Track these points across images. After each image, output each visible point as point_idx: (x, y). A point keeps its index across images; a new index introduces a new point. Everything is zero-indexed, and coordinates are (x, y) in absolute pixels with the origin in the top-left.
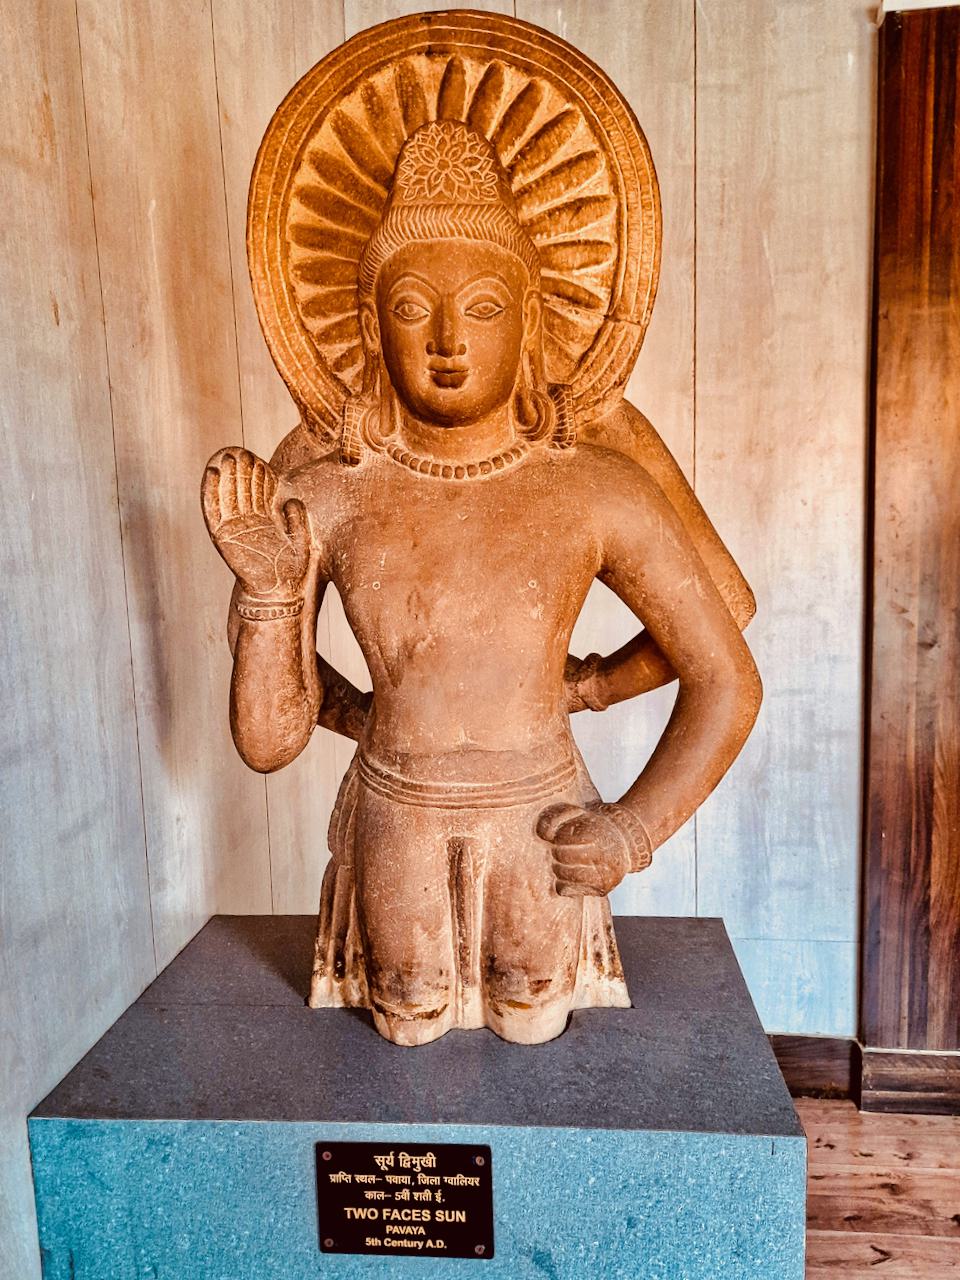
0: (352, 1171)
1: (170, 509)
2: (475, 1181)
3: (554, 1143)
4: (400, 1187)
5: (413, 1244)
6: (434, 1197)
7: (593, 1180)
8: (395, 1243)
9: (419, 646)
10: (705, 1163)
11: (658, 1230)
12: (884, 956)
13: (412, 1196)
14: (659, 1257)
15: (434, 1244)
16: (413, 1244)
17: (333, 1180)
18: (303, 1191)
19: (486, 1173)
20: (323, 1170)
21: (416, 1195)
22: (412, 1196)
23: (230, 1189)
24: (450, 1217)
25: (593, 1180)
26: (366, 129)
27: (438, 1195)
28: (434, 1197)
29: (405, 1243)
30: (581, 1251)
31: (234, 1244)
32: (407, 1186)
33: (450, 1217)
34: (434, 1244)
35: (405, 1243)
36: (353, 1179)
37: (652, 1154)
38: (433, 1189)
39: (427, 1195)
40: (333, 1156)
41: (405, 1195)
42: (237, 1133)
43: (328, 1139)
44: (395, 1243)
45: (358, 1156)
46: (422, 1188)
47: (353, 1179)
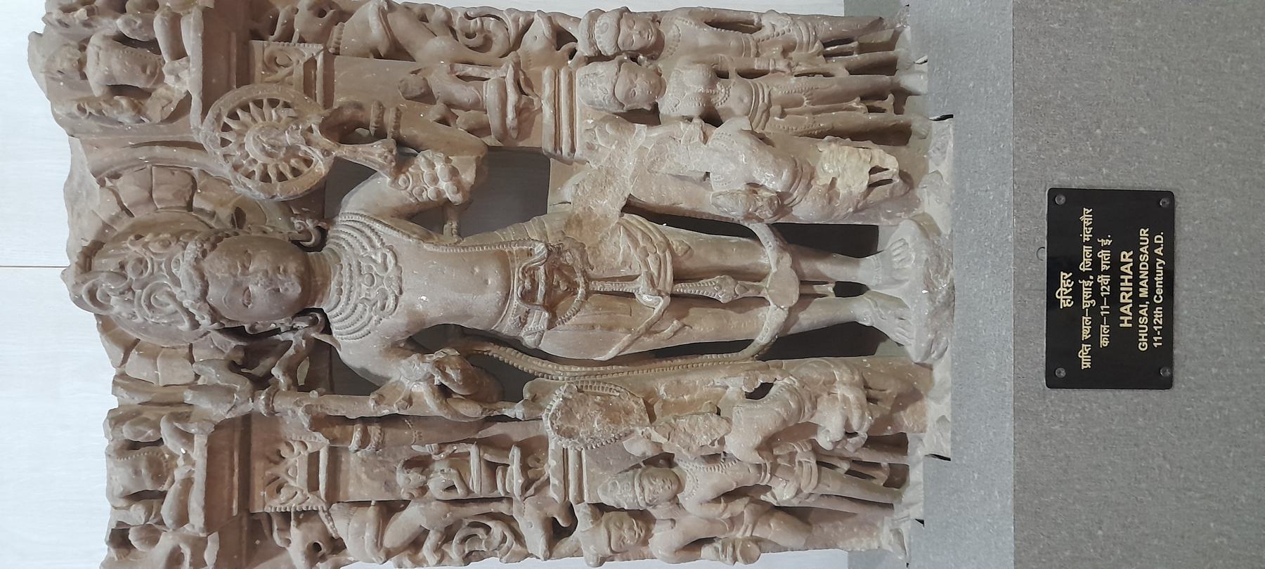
0: (1078, 343)
3: (1104, 170)
4: (1096, 288)
5: (1160, 270)
6: (1106, 248)
7: (1142, 129)
8: (1159, 292)
9: (543, 325)
10: (1119, 8)
11: (1193, 61)
13: (1105, 273)
14: (1222, 61)
15: (1159, 245)
16: (1160, 270)
17: (1088, 365)
18: (1164, 458)
21: (1104, 267)
22: (1105, 273)
23: (1163, 543)
25: (1142, 129)
27: (1104, 242)
28: (1106, 248)
29: (1159, 279)
30: (1220, 146)
31: (1225, 540)
34: (1159, 245)
35: (1159, 279)
36: (1086, 342)
37: (1110, 64)
39: (1104, 255)
41: (1104, 280)
42: (1100, 532)
43: (1042, 368)
44: (1159, 292)
46: (1096, 262)
47: (1086, 342)
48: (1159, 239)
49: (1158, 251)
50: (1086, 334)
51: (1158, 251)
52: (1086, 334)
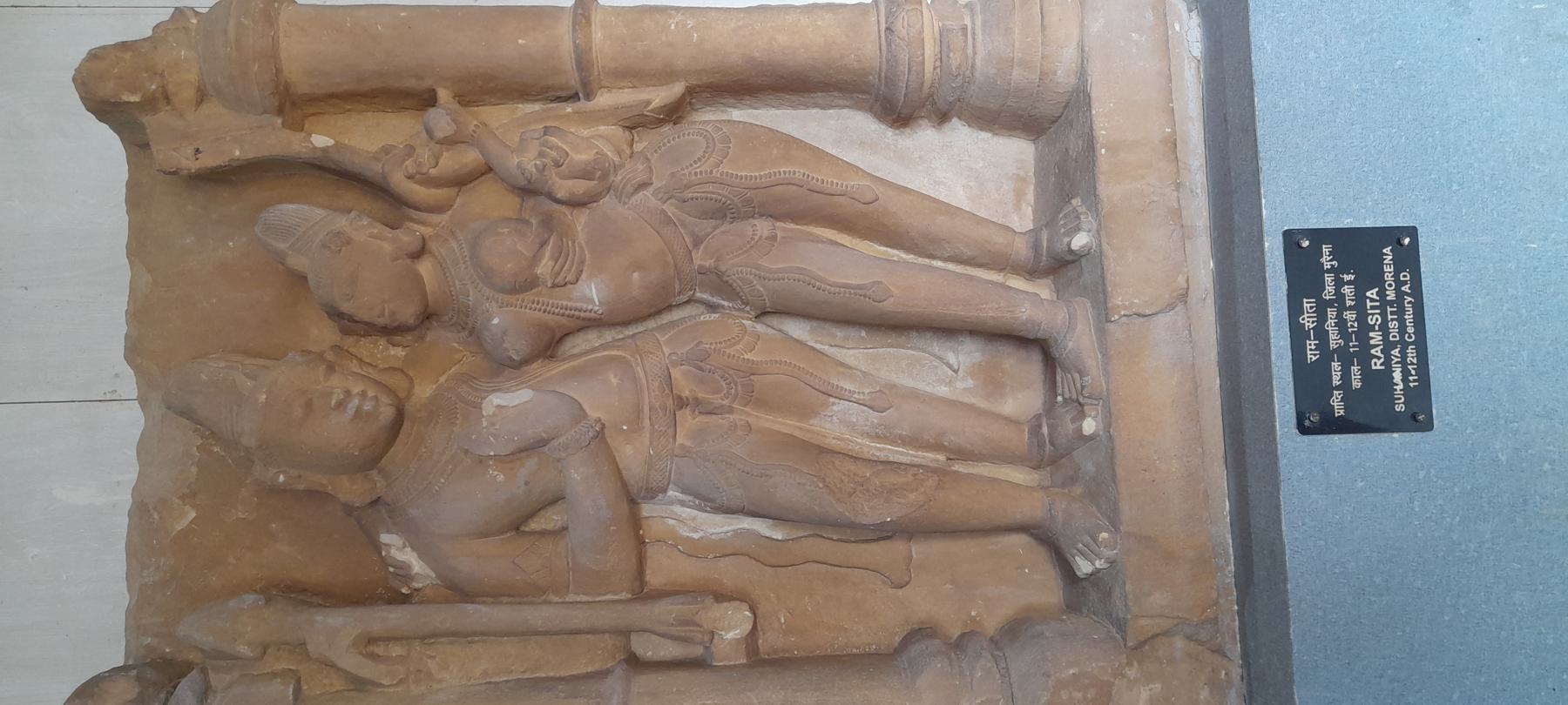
1: (978, 63)
2: (1326, 249)
6: (1349, 283)
8: (1411, 330)
12: (1172, 145)
15: (1405, 283)
17: (1159, 686)
19: (1319, 236)
20: (1392, 235)
21: (1349, 303)
22: (1351, 308)
24: (1372, 308)
26: (1001, 240)
27: (1347, 277)
28: (1349, 283)
29: (1409, 317)
32: (1339, 316)
33: (1372, 308)
35: (1409, 317)
36: (1337, 388)
38: (1339, 284)
40: (1317, 420)
44: (1411, 330)
45: (1310, 382)
46: (1340, 297)
47: (1337, 388)
48: (1405, 276)
49: (1406, 288)
50: (1336, 381)
51: (1406, 288)
52: (1336, 381)
